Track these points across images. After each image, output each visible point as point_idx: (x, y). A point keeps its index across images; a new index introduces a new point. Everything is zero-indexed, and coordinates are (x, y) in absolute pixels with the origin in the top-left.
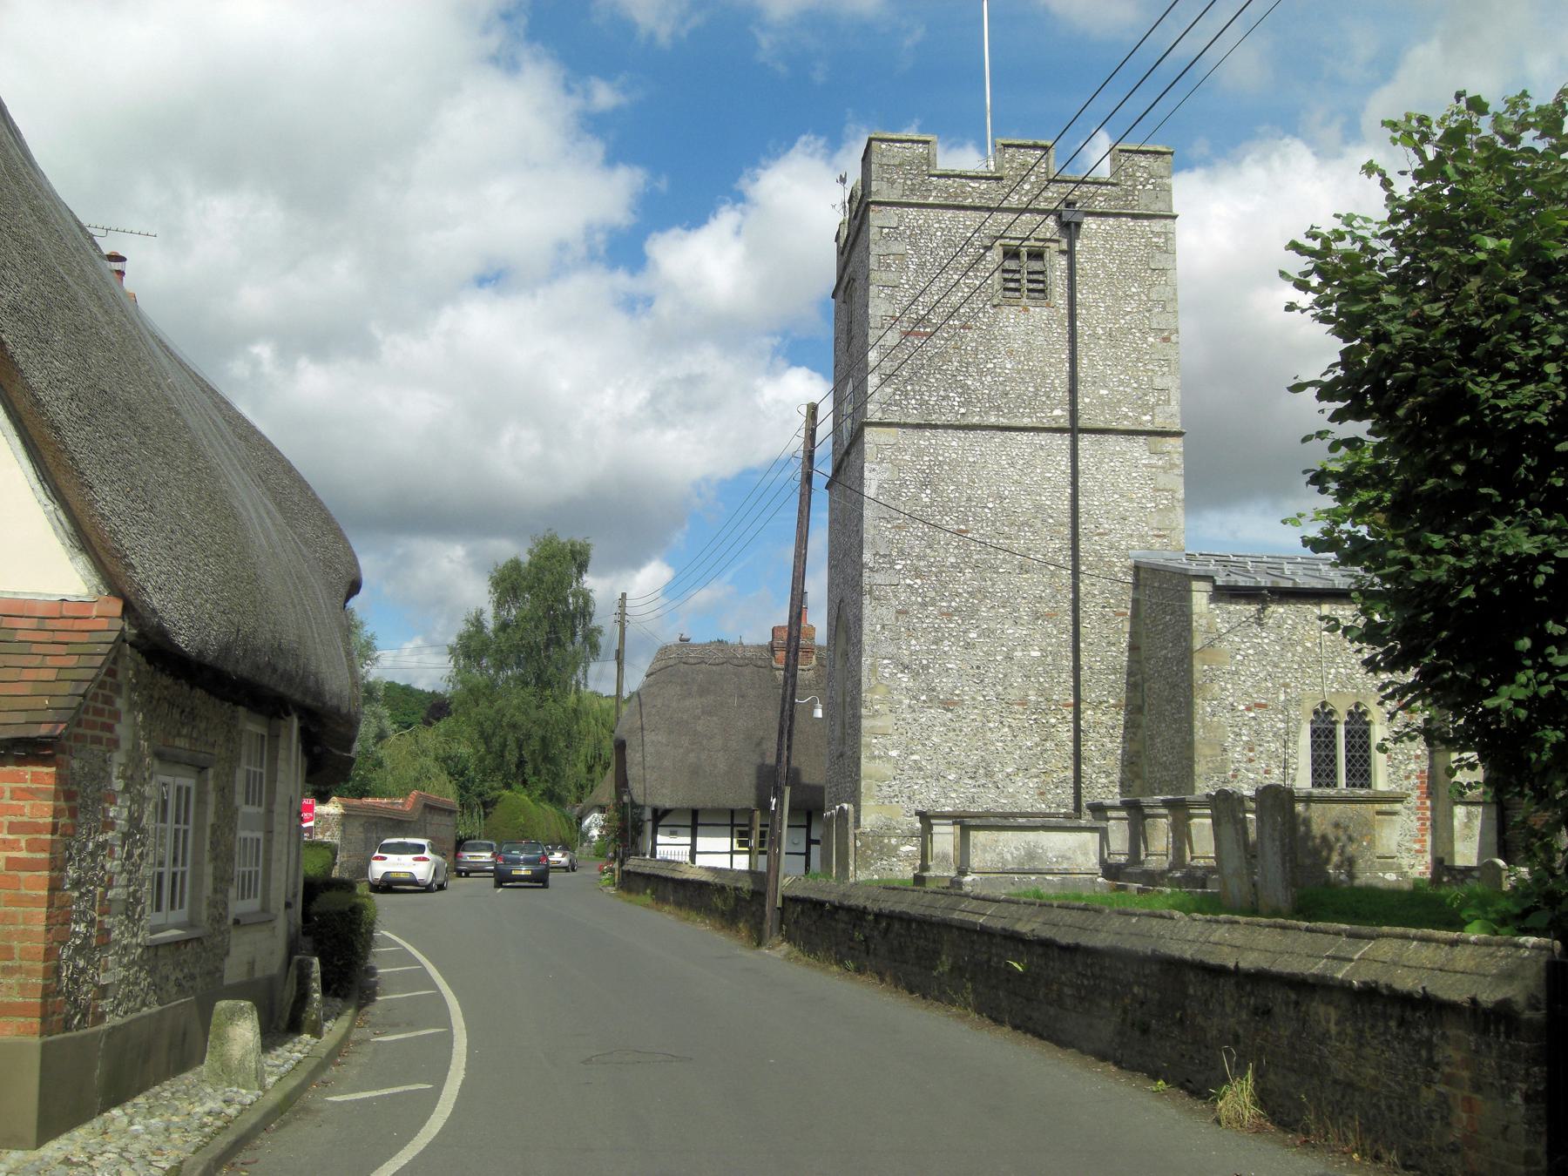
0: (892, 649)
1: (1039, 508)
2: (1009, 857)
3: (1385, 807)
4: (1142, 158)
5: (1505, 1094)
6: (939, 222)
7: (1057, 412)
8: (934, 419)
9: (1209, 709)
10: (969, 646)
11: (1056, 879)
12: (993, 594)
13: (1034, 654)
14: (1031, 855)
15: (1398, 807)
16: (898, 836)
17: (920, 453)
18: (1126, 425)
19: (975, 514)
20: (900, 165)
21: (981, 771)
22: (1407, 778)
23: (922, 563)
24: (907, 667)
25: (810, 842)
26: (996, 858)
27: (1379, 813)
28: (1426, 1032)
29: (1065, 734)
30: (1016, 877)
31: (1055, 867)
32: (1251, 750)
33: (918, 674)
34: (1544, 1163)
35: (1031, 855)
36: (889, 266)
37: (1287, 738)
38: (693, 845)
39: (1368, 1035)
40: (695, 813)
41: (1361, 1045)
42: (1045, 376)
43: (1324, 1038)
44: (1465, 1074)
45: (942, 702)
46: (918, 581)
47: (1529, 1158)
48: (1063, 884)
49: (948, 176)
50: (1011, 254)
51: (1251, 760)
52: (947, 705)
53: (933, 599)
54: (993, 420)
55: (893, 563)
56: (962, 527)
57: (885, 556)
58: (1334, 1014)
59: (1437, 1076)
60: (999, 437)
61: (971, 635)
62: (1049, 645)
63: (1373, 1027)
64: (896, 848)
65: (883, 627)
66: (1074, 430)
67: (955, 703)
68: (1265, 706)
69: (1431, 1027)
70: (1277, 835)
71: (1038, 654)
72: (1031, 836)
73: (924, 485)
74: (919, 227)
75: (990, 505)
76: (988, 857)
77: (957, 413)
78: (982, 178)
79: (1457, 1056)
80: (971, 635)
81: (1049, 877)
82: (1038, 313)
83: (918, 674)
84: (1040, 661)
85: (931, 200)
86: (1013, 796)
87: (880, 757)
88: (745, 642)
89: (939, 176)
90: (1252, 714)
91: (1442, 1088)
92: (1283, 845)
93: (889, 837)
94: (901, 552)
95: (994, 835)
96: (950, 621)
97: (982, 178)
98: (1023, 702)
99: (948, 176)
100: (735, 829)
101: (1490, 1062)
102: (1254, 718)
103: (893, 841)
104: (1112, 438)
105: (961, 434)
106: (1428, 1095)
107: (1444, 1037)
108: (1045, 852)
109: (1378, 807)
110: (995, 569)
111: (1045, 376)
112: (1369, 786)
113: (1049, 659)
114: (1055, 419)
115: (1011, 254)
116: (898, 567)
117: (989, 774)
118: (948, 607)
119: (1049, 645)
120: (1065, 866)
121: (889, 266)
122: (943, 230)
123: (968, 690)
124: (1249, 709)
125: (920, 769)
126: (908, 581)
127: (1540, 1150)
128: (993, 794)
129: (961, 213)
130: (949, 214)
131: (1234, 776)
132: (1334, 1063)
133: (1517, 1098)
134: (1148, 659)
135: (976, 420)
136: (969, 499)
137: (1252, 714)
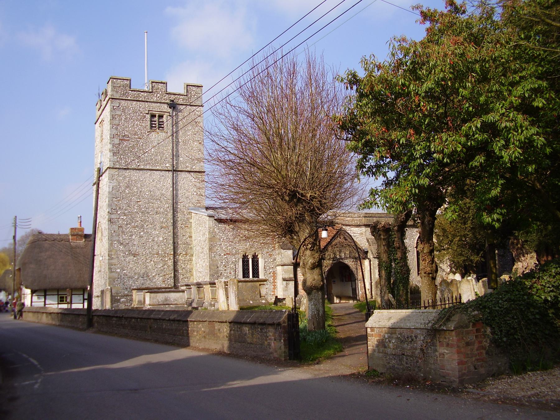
0: (117, 238)
1: (163, 195)
2: (160, 300)
3: (262, 283)
4: (194, 87)
5: (280, 340)
6: (132, 105)
7: (167, 165)
8: (129, 167)
9: (213, 255)
10: (141, 237)
11: (173, 306)
12: (148, 221)
13: (160, 239)
14: (166, 300)
15: (265, 283)
16: (120, 296)
17: (125, 177)
18: (189, 169)
19: (142, 196)
20: (120, 87)
21: (145, 275)
22: (270, 274)
23: (126, 212)
24: (122, 244)
25: (84, 299)
26: (156, 301)
27: (260, 285)
28: (265, 330)
29: (171, 263)
30: (162, 306)
31: (173, 303)
32: (225, 267)
33: (125, 246)
34: (288, 353)
35: (166, 300)
36: (116, 118)
37: (235, 263)
38: (45, 302)
39: (254, 332)
40: (72, 290)
41: (253, 335)
42: (164, 154)
43: (246, 334)
44: (273, 338)
45: (133, 254)
46: (125, 217)
47: (285, 352)
48: (176, 307)
49: (135, 91)
50: (153, 116)
51: (225, 270)
52: (135, 255)
53: (130, 222)
54: (148, 167)
55: (117, 212)
56: (138, 200)
57: (115, 209)
58: (247, 329)
59: (268, 339)
60: (149, 172)
61: (141, 234)
62: (165, 236)
63: (255, 331)
64: (120, 299)
65: (114, 231)
66: (175, 171)
67: (137, 255)
68: (229, 254)
69: (266, 329)
70: (234, 291)
71: (162, 239)
72: (166, 294)
73: (128, 187)
74: (125, 106)
75: (147, 193)
76: (154, 301)
77: (137, 165)
78: (145, 92)
79: (271, 334)
80: (141, 234)
81: (171, 306)
82: (162, 135)
83: (125, 246)
84: (162, 241)
85: (129, 98)
86: (155, 282)
87: (114, 272)
88: (61, 233)
89: (132, 91)
90: (226, 257)
91: (268, 341)
92: (235, 294)
93: (117, 297)
94: (120, 208)
95: (155, 295)
96: (135, 229)
97: (145, 92)
98: (158, 254)
99: (135, 91)
100: (59, 296)
101: (277, 335)
102: (226, 258)
103: (119, 298)
104: (183, 173)
105: (138, 171)
106: (266, 343)
107: (269, 331)
108: (170, 299)
109: (260, 283)
110: (148, 213)
111: (164, 154)
112: (258, 278)
113: (165, 240)
114: (167, 167)
115: (153, 116)
116: (119, 213)
117: (148, 276)
118: (134, 225)
119: (165, 236)
120: (176, 302)
121: (116, 118)
122: (133, 108)
123: (140, 251)
124: (225, 255)
125: (126, 275)
126: (122, 217)
127: (287, 350)
128: (149, 282)
129: (139, 103)
130: (135, 103)
131: (221, 275)
132: (248, 339)
133: (282, 341)
134: (195, 240)
135: (142, 167)
136: (141, 192)
137: (226, 257)
